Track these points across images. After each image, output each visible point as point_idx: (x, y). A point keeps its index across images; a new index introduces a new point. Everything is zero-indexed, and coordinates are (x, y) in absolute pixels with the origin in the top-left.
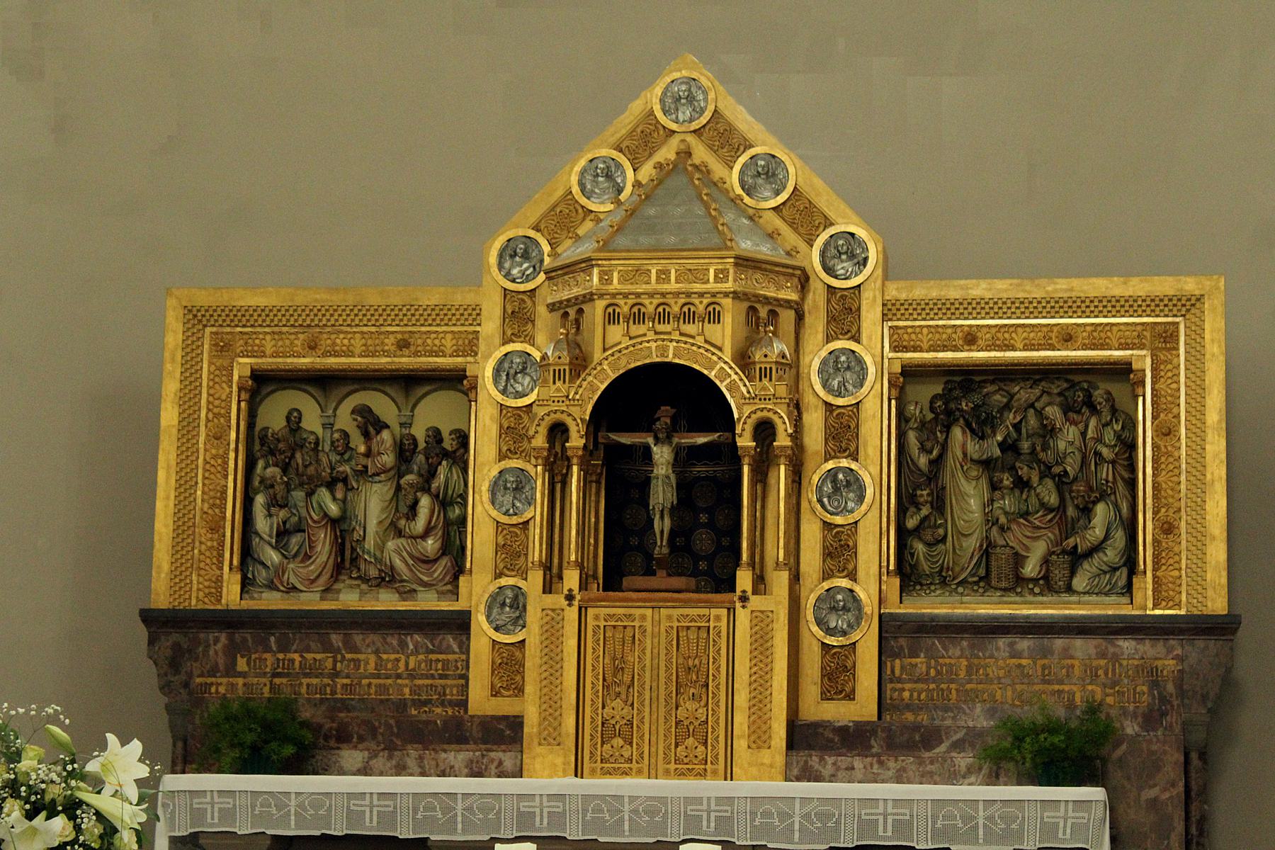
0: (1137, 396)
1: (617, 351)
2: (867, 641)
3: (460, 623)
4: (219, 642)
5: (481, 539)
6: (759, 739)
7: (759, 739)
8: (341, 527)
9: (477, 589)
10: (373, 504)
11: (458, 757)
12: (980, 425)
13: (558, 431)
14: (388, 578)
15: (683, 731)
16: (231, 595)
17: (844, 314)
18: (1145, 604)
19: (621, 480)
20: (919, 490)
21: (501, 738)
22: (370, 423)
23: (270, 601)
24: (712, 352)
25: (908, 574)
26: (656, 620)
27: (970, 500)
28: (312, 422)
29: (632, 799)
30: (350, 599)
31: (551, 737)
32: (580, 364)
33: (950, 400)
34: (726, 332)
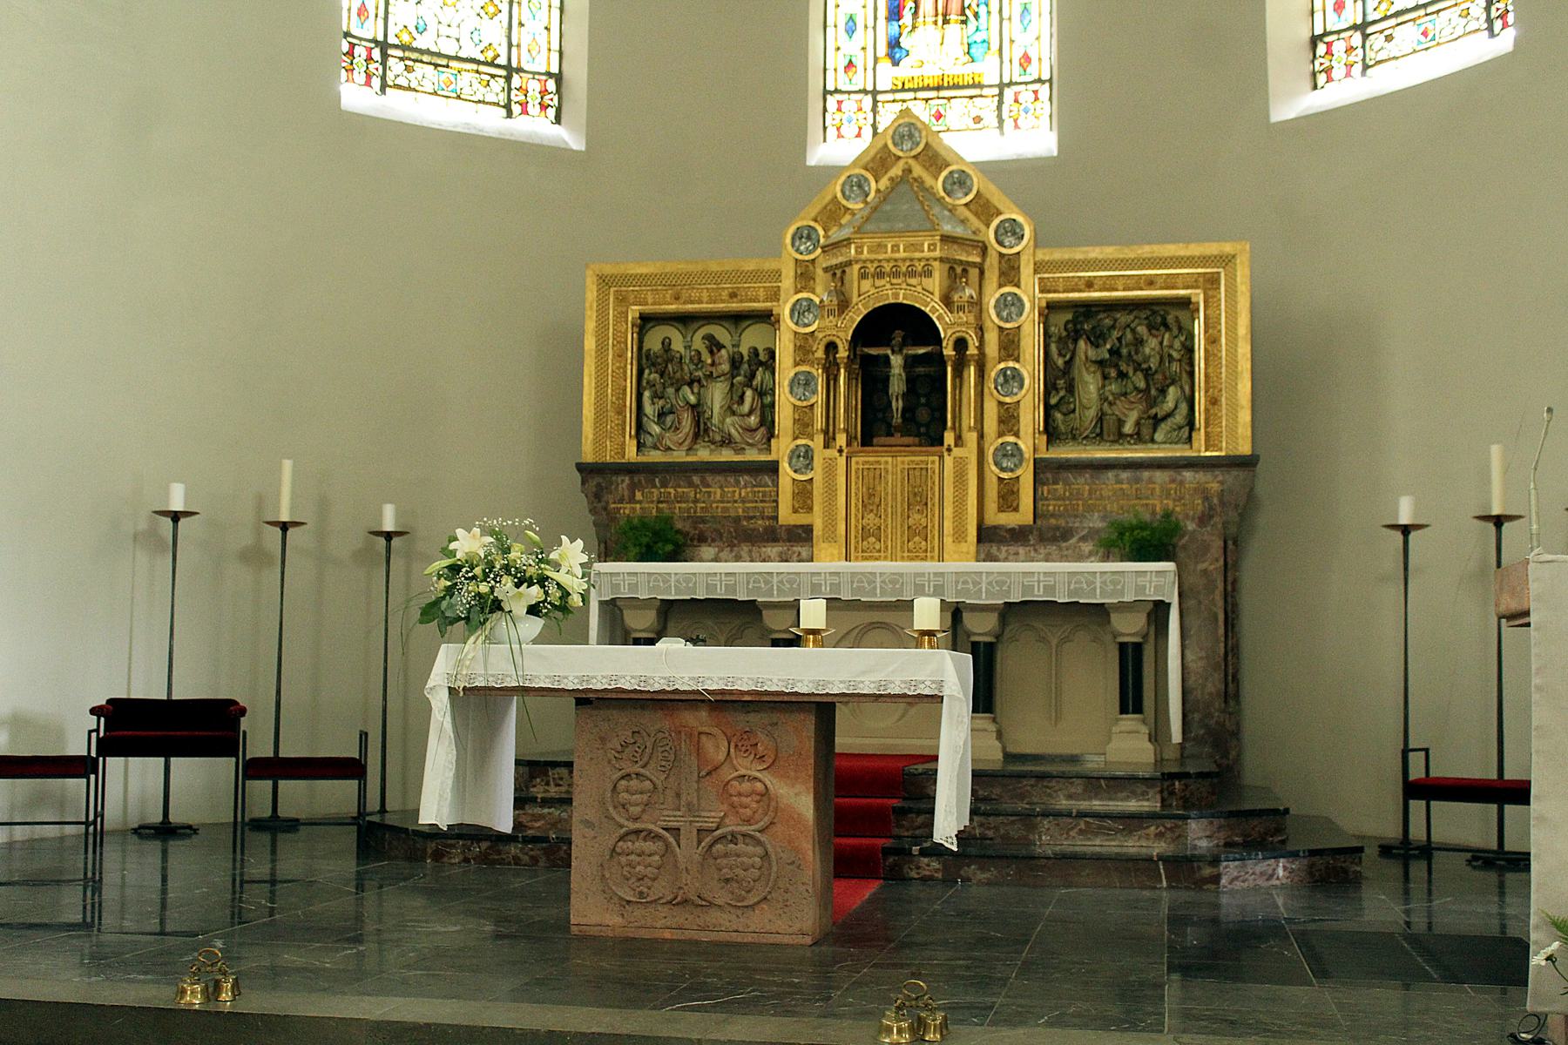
1: (868, 296)
2: (1026, 475)
3: (773, 468)
4: (624, 482)
7: (960, 536)
8: (697, 409)
9: (782, 448)
10: (717, 395)
11: (772, 550)
12: (1096, 339)
14: (727, 441)
15: (912, 532)
16: (631, 454)
17: (1009, 270)
18: (1199, 448)
19: (871, 377)
20: (1058, 380)
22: (714, 345)
23: (655, 456)
24: (927, 296)
25: (1052, 433)
26: (894, 463)
27: (1090, 385)
28: (678, 345)
30: (704, 454)
31: (830, 537)
32: (844, 305)
34: (936, 283)
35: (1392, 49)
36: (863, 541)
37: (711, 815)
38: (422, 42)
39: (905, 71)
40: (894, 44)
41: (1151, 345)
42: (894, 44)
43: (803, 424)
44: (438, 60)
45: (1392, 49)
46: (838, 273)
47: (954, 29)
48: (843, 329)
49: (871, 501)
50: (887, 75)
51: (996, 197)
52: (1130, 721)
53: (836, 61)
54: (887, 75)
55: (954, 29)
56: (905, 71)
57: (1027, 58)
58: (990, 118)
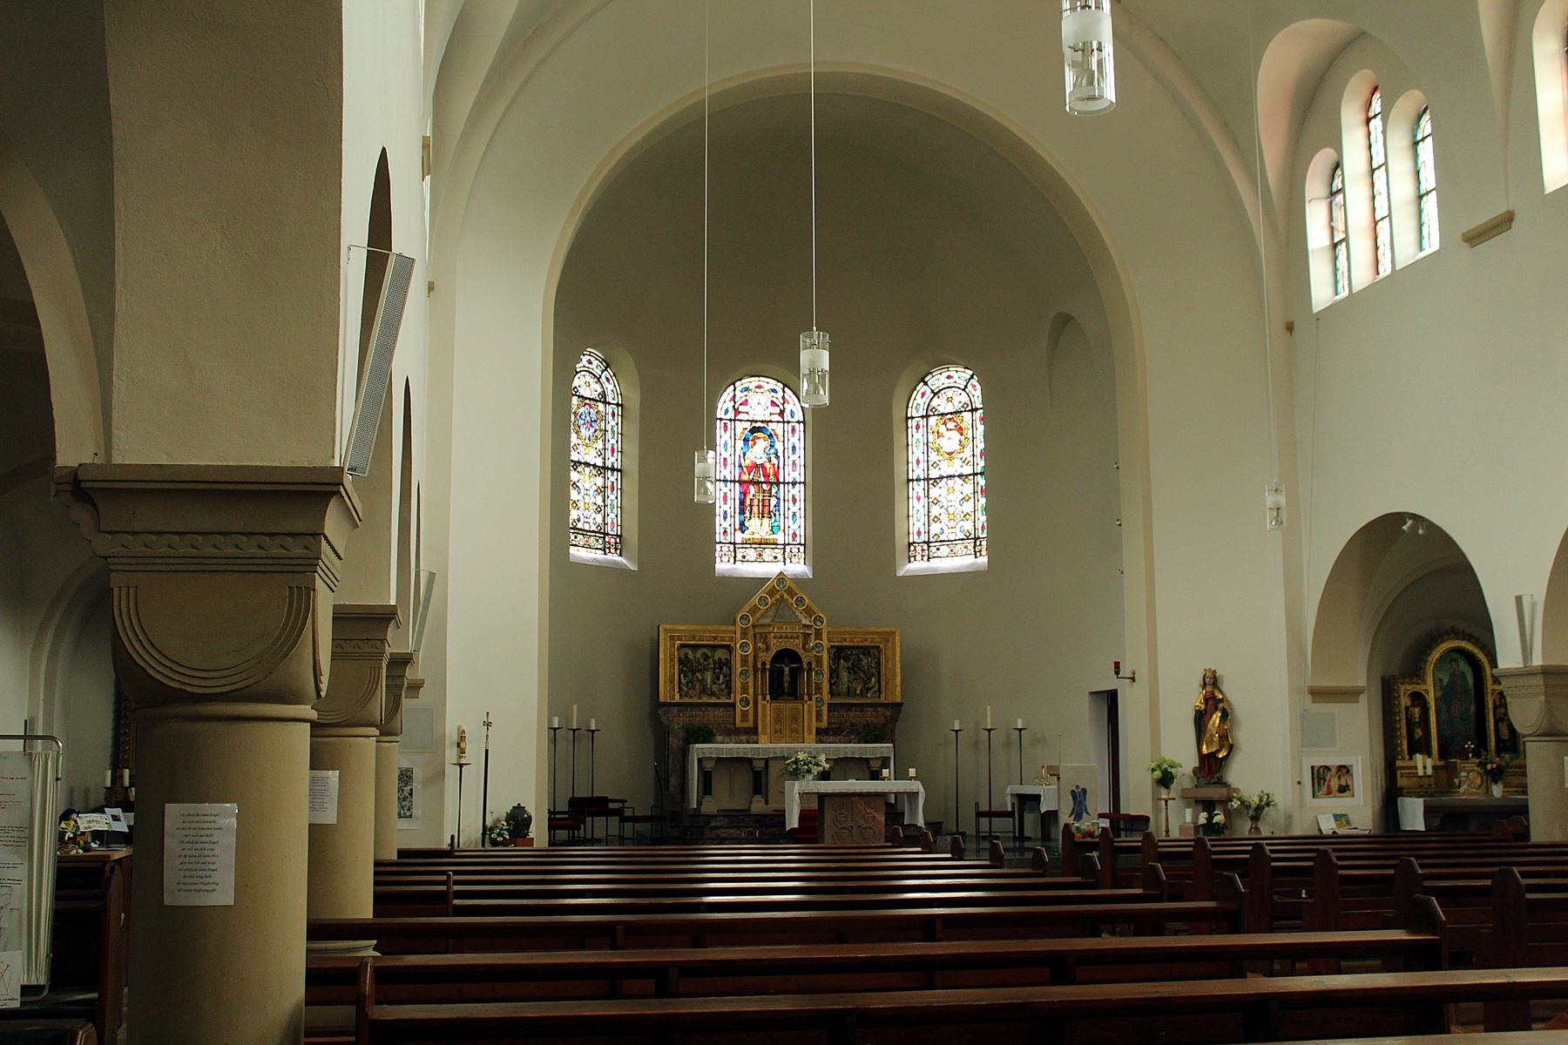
0: (1417, 917)
1: (776, 646)
2: (825, 708)
3: (734, 705)
4: (675, 710)
5: (738, 682)
6: (810, 732)
7: (810, 732)
8: (702, 681)
9: (738, 696)
10: (709, 676)
11: (743, 738)
12: (846, 659)
13: (764, 664)
14: (713, 694)
15: (792, 731)
16: (677, 699)
17: (818, 634)
18: (882, 699)
19: (776, 676)
20: (834, 673)
21: (752, 733)
22: (706, 658)
23: (686, 700)
24: (795, 645)
25: (831, 693)
26: (787, 707)
27: (845, 675)
28: (690, 656)
29: (1329, 793)
30: (705, 700)
31: (764, 733)
32: (768, 649)
33: (838, 653)
34: (799, 641)
35: (939, 553)
36: (777, 735)
37: (861, 822)
38: (580, 526)
39: (747, 535)
40: (742, 524)
41: (865, 662)
42: (742, 524)
43: (745, 689)
44: (584, 532)
45: (939, 553)
46: (765, 637)
47: (766, 520)
48: (767, 657)
49: (778, 720)
50: (739, 537)
51: (814, 608)
52: (758, 798)
53: (719, 530)
54: (739, 537)
55: (766, 520)
56: (747, 535)
57: (795, 535)
58: (780, 557)
